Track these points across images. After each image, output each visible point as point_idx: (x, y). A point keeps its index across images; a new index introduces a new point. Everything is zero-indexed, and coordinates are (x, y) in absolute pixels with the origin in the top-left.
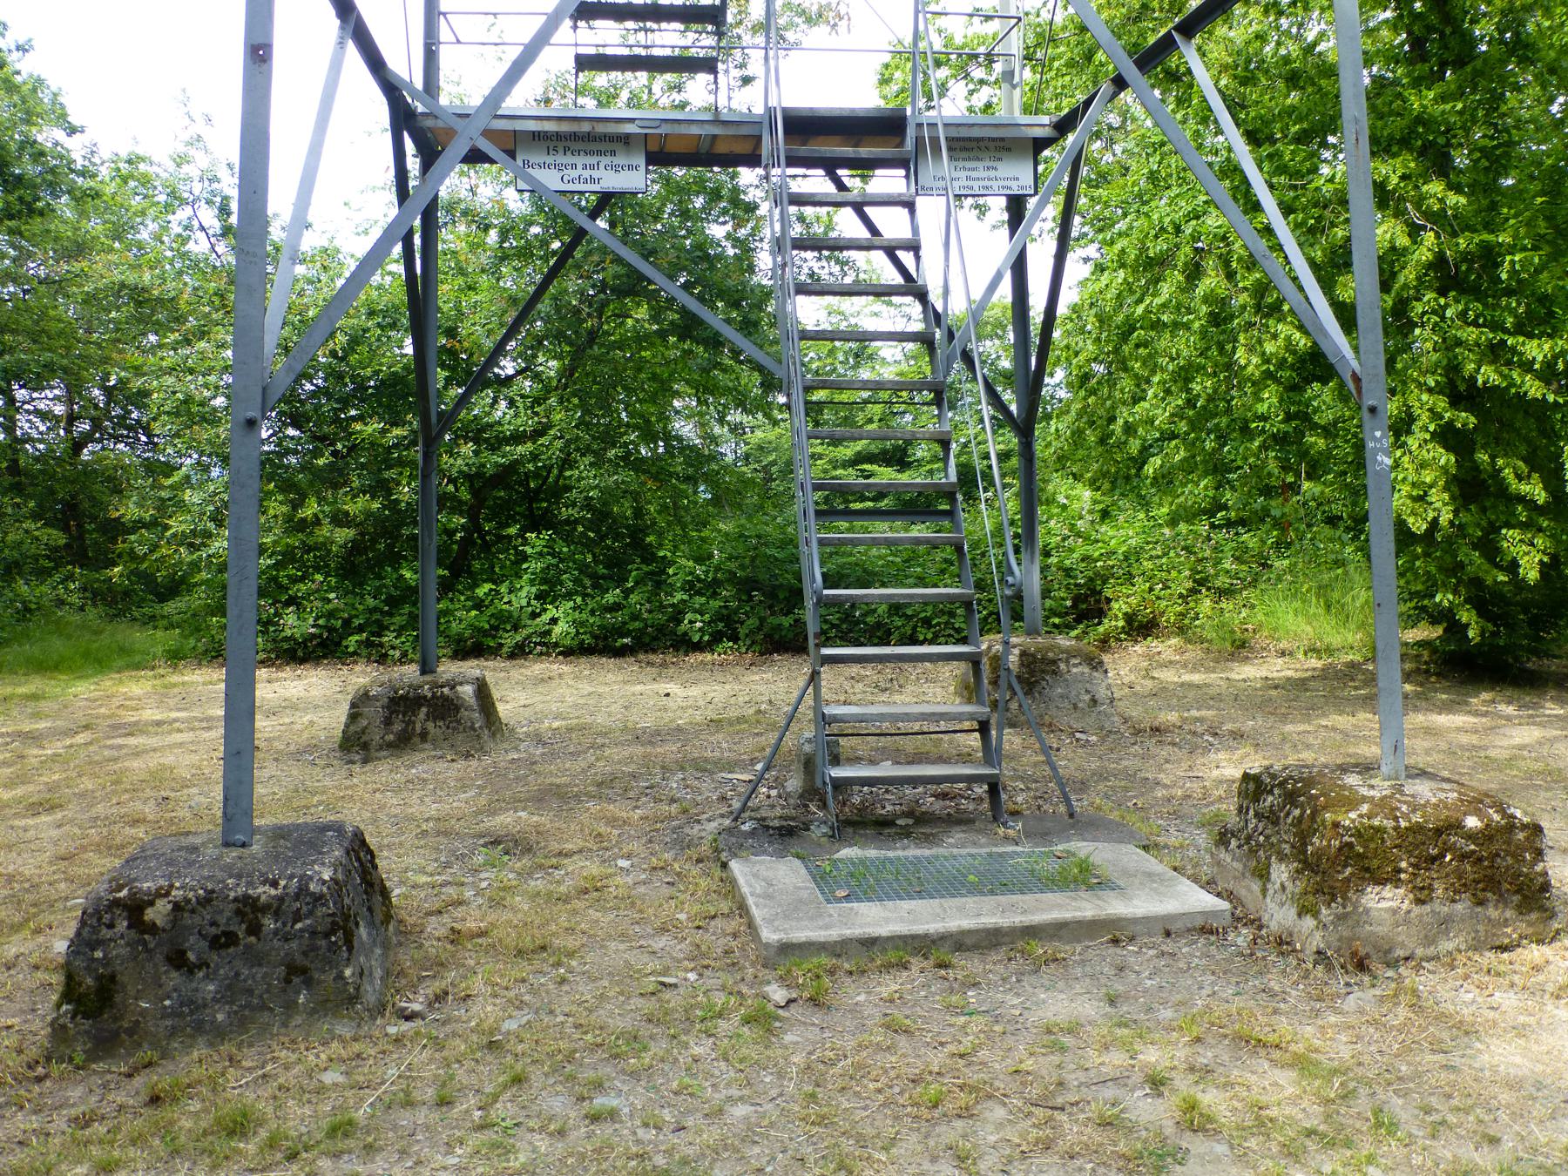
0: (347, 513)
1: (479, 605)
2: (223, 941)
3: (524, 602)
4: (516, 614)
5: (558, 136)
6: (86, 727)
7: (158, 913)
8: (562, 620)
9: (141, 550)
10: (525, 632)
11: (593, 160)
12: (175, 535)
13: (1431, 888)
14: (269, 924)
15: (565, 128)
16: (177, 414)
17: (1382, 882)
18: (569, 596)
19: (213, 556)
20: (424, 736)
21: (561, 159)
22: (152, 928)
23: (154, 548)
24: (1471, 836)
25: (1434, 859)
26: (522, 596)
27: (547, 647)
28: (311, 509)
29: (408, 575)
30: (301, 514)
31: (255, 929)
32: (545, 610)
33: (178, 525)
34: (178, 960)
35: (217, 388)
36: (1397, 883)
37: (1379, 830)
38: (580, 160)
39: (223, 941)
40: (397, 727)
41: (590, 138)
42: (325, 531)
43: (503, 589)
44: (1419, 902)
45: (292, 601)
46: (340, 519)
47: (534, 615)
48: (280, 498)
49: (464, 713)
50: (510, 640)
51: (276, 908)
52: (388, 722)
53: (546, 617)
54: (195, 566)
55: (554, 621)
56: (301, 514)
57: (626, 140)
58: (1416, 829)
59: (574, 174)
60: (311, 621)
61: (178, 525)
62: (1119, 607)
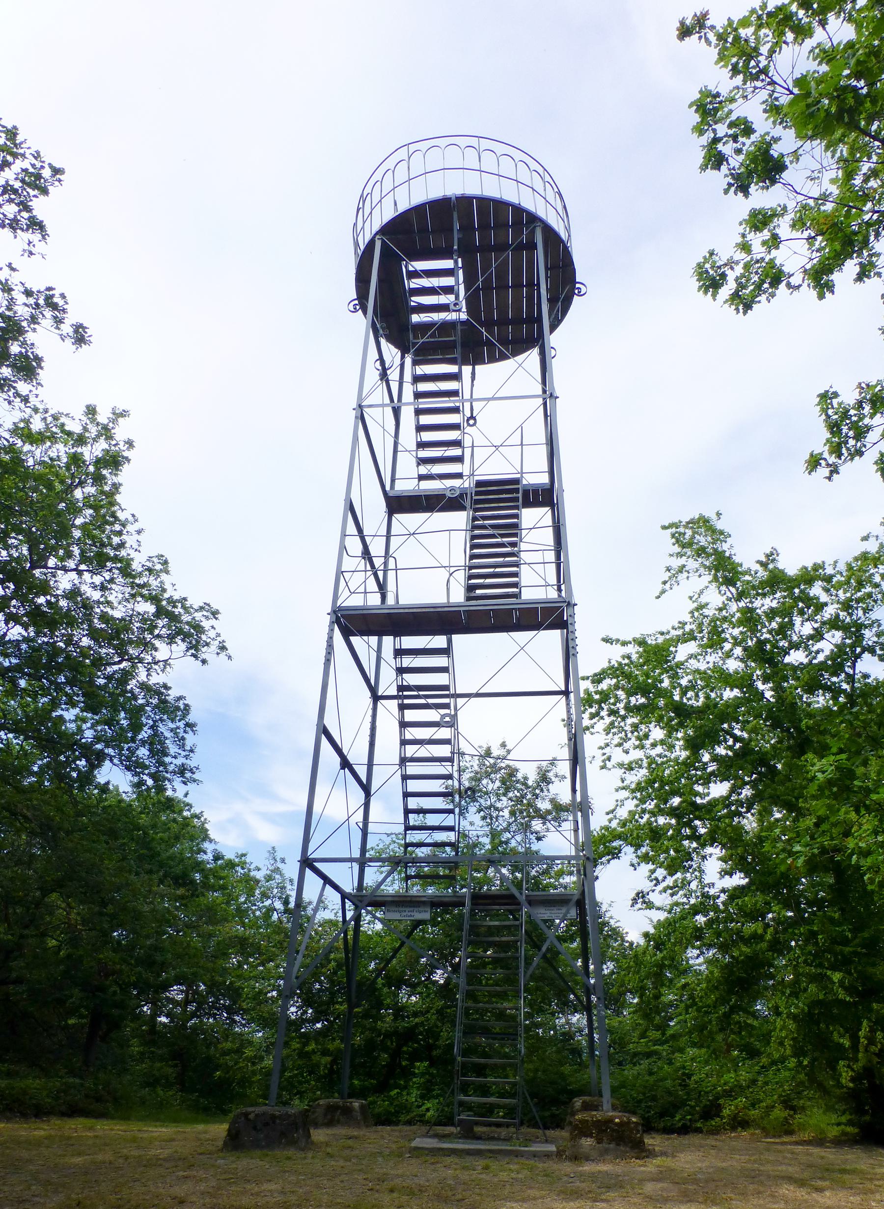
0: (329, 1050)
1: (391, 1099)
2: (266, 1124)
3: (414, 1100)
4: (409, 1106)
5: (400, 902)
6: (822, 82)
7: (251, 1116)
8: (431, 1108)
9: (231, 1063)
10: (412, 1115)
11: (412, 909)
12: (246, 1057)
13: (602, 1140)
14: (278, 1121)
15: (401, 899)
16: (254, 999)
17: (586, 1136)
18: (436, 1097)
19: (263, 1068)
20: (338, 1122)
21: (401, 909)
22: (250, 1120)
23: (236, 1063)
24: (617, 1124)
25: (604, 1131)
26: (413, 1096)
27: (421, 1120)
28: (312, 1046)
29: (356, 1082)
30: (307, 1049)
31: (274, 1122)
32: (423, 1104)
33: (248, 1052)
34: (255, 1128)
35: (274, 986)
36: (592, 1137)
37: (587, 1121)
38: (407, 909)
39: (266, 1124)
40: (329, 1117)
41: (411, 902)
42: (316, 1058)
43: (404, 1093)
44: (598, 1143)
45: (299, 1093)
46: (325, 1052)
47: (419, 1107)
48: (297, 1040)
49: (354, 1113)
50: (403, 1118)
51: (280, 1117)
52: (325, 1115)
53: (424, 1108)
54: (254, 1073)
55: (428, 1110)
56: (307, 1049)
57: (424, 903)
58: (599, 1121)
59: (405, 914)
60: (306, 1103)
61: (248, 1052)
62: (726, 1112)
